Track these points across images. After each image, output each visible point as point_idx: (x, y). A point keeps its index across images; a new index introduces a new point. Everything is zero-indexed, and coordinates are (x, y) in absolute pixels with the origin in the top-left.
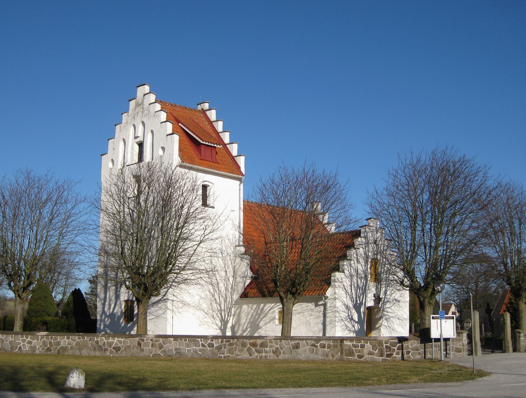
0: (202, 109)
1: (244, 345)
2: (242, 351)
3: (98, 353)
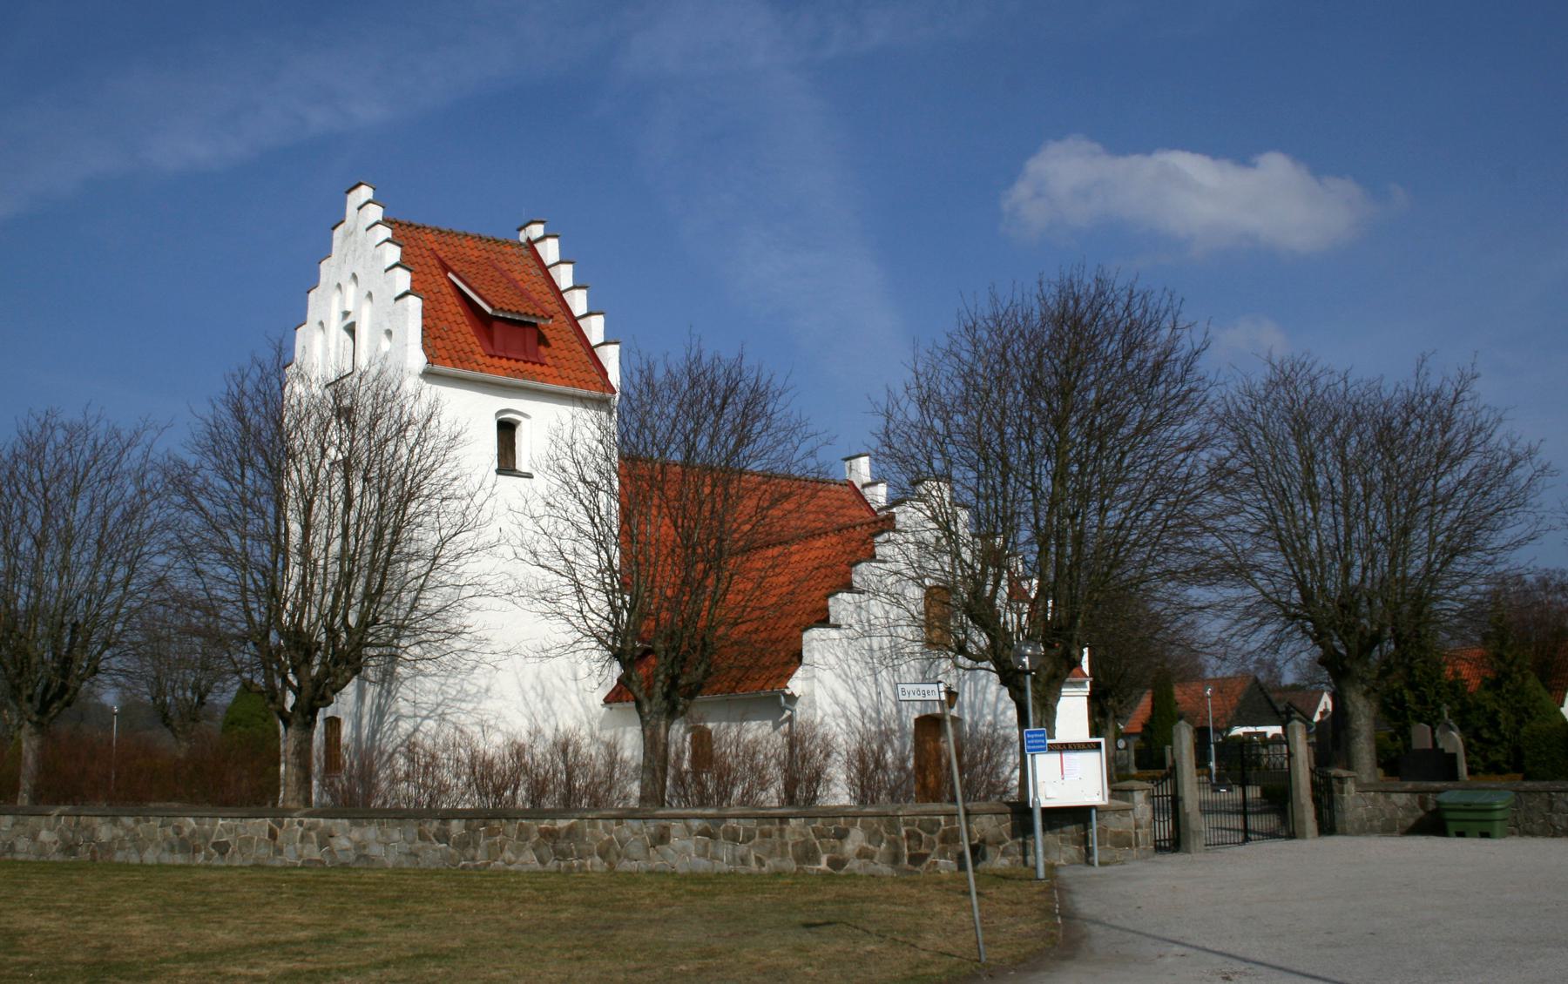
0: (528, 239)
1: (523, 834)
2: (519, 851)
3: (179, 859)
